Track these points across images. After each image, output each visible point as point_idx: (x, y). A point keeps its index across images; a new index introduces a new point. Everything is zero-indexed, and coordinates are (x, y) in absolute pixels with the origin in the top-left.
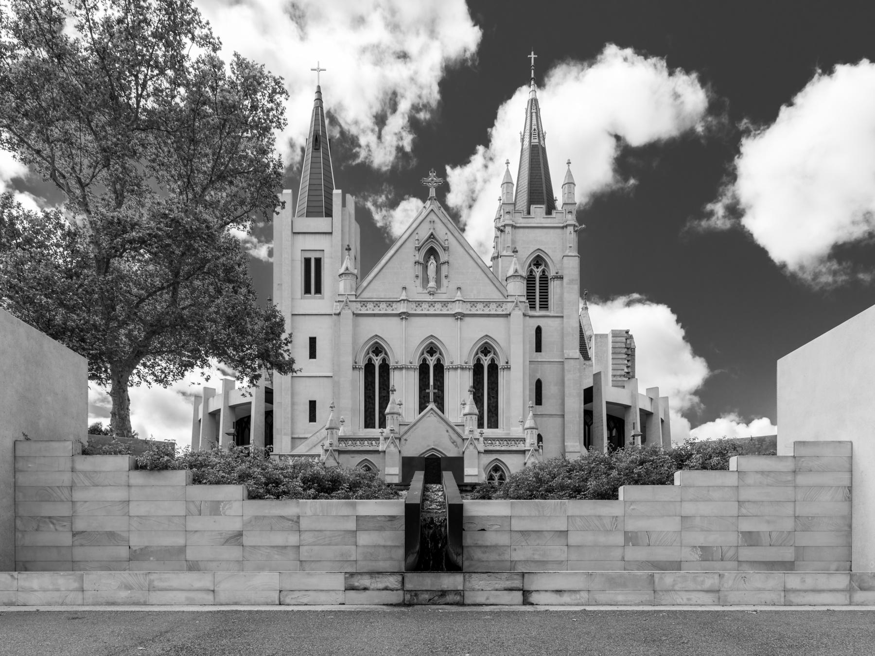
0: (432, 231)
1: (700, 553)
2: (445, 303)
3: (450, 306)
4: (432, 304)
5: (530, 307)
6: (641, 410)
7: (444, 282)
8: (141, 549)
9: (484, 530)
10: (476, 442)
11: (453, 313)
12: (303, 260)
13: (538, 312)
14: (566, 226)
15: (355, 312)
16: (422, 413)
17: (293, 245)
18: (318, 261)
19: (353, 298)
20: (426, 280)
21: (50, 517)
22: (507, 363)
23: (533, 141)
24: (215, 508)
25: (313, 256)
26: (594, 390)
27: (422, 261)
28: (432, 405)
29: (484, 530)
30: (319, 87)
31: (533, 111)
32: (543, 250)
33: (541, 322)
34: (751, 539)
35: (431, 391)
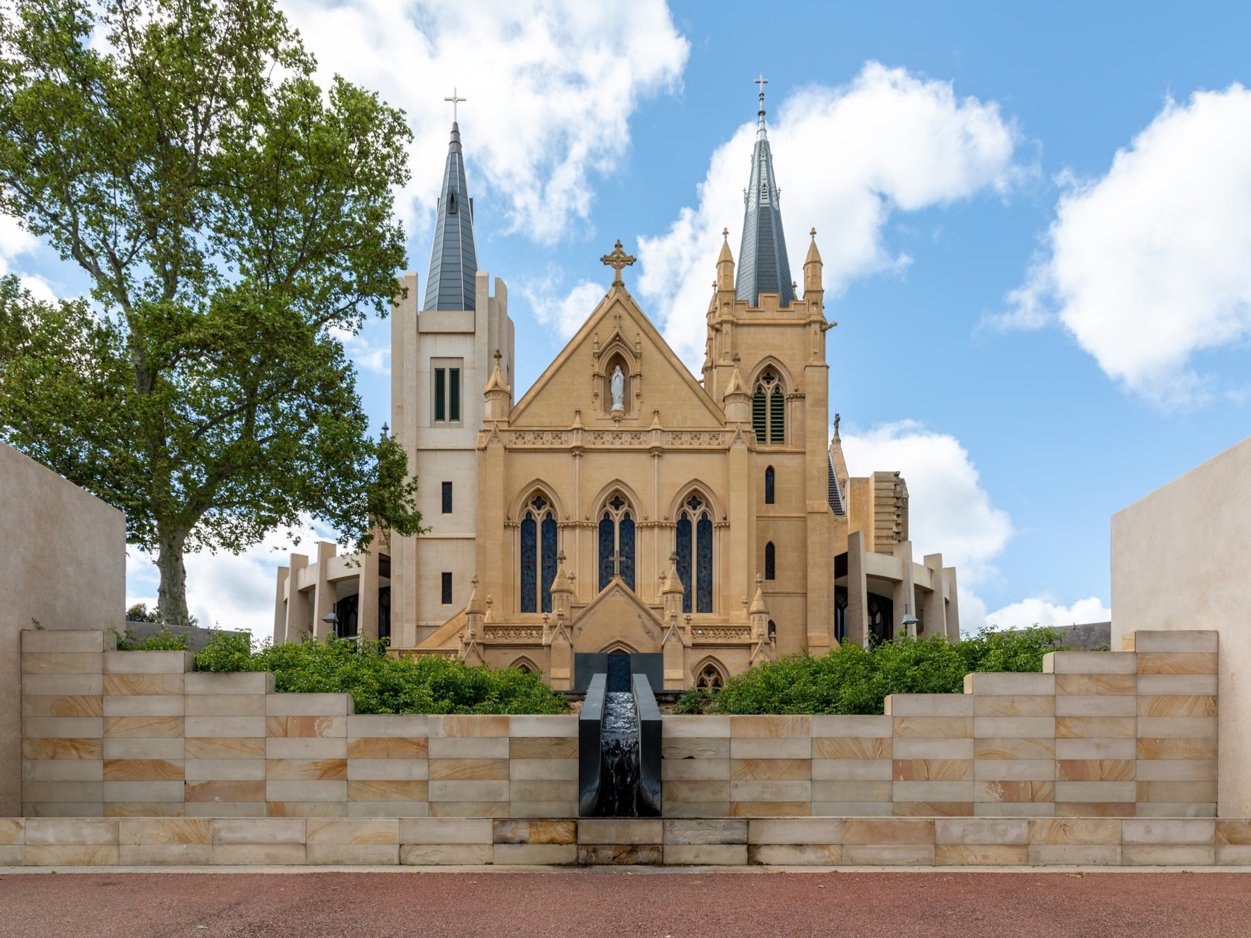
0: (617, 330)
1: (1000, 790)
2: (636, 434)
3: (643, 437)
4: (617, 434)
5: (758, 440)
6: (916, 586)
7: (636, 403)
8: (202, 786)
9: (691, 758)
10: (680, 632)
11: (648, 447)
12: (434, 371)
13: (769, 446)
14: (809, 324)
15: (508, 446)
16: (604, 591)
17: (418, 350)
18: (455, 373)
19: (505, 426)
20: (609, 401)
21: (71, 740)
22: (725, 519)
23: (762, 201)
24: (308, 727)
25: (447, 366)
26: (850, 557)
27: (603, 373)
28: (617, 580)
29: (691, 758)
30: (456, 124)
31: (762, 158)
32: (777, 357)
33: (774, 461)
34: (1073, 770)
35: (616, 559)
